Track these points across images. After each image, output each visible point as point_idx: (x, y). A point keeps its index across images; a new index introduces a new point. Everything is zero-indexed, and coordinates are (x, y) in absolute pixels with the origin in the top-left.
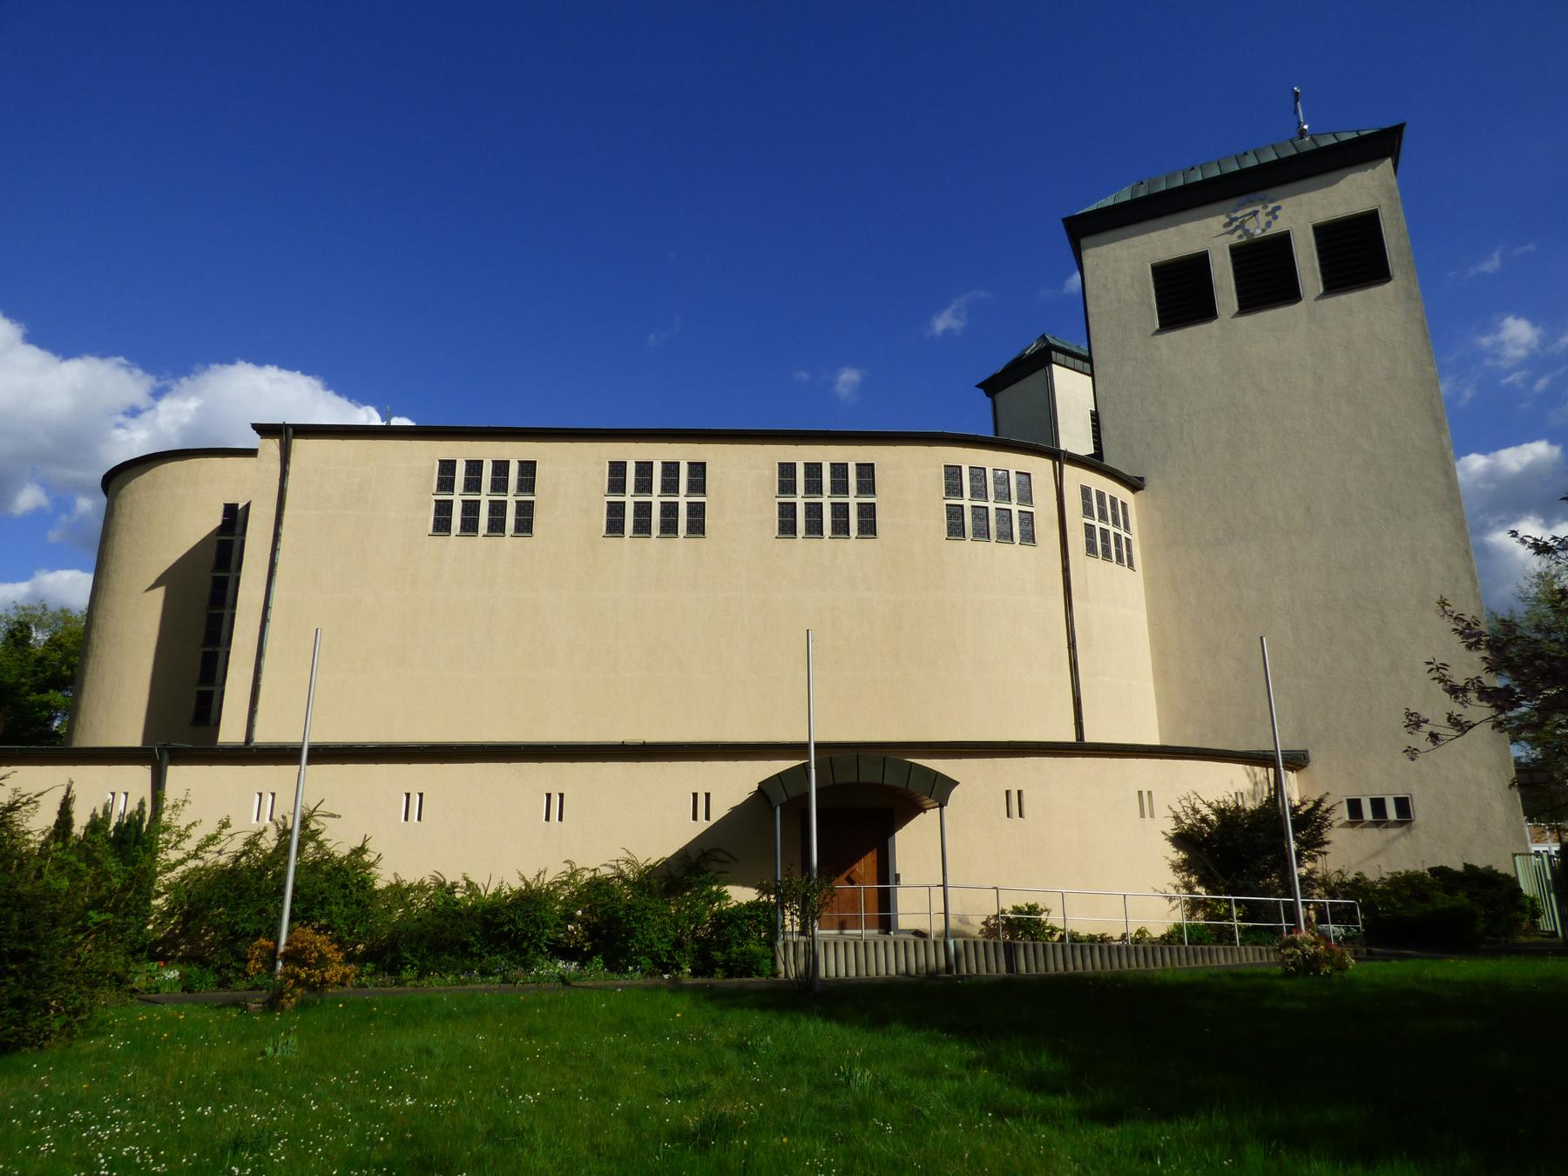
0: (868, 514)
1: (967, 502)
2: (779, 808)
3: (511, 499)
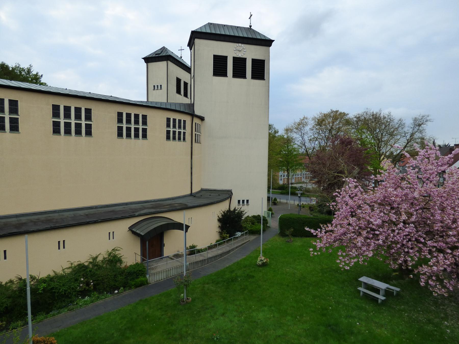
0: (89, 128)
1: (171, 129)
2: (147, 242)
3: (83, 123)
